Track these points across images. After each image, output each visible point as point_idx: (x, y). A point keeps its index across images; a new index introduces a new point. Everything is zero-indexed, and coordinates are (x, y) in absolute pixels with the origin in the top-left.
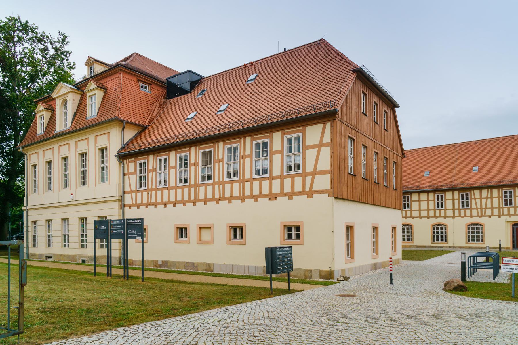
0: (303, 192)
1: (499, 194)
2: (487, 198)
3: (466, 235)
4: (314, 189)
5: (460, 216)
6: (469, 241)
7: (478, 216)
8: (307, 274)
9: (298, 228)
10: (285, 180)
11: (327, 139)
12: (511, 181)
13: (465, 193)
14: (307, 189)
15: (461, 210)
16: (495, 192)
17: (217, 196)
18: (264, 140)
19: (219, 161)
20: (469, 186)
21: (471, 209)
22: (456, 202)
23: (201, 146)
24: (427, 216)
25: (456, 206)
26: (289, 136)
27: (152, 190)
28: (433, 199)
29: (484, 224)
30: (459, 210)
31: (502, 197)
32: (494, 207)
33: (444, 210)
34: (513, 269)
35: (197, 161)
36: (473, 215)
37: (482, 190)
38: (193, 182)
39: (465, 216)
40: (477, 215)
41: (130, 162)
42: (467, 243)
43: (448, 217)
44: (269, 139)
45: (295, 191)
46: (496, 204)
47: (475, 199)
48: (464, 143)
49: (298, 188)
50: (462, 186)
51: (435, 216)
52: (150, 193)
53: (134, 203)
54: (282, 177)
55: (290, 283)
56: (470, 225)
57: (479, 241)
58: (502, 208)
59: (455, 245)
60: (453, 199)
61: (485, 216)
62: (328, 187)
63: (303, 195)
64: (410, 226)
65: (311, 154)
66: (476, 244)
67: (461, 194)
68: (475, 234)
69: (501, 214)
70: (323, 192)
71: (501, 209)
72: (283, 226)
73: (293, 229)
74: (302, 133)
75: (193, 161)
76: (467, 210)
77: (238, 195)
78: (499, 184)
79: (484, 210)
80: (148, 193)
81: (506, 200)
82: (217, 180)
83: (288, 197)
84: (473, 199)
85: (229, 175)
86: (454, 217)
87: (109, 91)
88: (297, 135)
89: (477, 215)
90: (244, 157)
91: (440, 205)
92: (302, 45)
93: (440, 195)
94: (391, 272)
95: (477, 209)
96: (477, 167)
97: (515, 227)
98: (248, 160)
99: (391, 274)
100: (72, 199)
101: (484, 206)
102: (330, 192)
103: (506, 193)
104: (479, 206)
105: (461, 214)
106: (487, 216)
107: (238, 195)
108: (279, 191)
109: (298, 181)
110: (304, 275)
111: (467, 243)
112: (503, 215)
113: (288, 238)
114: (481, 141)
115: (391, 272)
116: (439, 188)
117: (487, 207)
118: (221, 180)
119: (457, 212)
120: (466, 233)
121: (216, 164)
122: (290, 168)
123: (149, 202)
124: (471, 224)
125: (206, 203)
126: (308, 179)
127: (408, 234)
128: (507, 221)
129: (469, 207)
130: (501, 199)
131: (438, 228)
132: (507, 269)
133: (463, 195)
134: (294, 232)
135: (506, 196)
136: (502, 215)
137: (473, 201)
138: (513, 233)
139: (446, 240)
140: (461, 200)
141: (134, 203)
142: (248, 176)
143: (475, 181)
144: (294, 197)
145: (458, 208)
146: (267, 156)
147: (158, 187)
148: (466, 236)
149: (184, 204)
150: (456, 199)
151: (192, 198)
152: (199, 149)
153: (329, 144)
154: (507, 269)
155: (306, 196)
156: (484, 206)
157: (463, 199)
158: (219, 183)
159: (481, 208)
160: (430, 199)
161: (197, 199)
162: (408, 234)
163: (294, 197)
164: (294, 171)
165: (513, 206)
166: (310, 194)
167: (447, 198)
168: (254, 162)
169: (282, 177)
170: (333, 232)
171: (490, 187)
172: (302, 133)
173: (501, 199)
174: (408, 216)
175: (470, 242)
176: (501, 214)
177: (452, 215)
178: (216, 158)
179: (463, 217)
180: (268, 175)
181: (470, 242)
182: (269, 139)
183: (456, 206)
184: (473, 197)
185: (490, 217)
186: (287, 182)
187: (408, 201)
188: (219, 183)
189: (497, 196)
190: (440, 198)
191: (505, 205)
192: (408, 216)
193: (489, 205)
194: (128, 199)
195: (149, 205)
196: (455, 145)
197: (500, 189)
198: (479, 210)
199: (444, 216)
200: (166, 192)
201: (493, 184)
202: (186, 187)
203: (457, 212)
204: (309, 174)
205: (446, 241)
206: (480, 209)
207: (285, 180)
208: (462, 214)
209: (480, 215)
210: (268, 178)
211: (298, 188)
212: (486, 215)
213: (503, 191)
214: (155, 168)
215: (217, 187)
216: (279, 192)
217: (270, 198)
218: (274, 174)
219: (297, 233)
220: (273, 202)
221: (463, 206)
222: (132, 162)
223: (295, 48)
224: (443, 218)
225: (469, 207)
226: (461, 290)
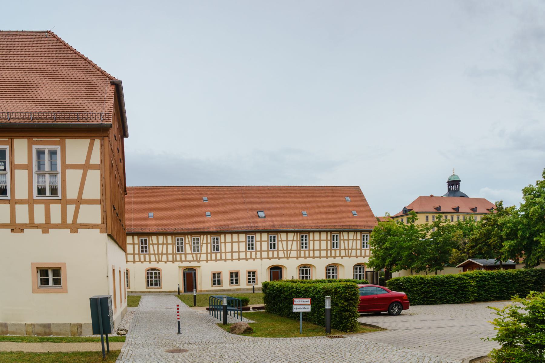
0: (63, 225)
1: (172, 241)
2: (163, 244)
3: (146, 280)
4: (79, 221)
5: (140, 261)
6: (148, 286)
7: (156, 261)
8: (75, 330)
9: (57, 272)
10: (35, 206)
11: (96, 159)
12: (182, 229)
13: (144, 238)
14: (70, 221)
15: (141, 255)
16: (169, 238)
18: (52, 147)
20: (148, 231)
21: (150, 254)
22: (136, 246)
24: (231, 258)
26: (41, 147)
28: (245, 241)
29: (161, 269)
30: (139, 254)
31: (175, 244)
32: (169, 253)
33: (219, 253)
34: (301, 308)
36: (152, 260)
37: (159, 236)
39: (145, 261)
40: (155, 260)
42: (147, 288)
44: (8, 146)
45: (51, 223)
46: (170, 251)
47: (344, 240)
48: (138, 188)
49: (56, 218)
50: (141, 231)
51: (268, 258)
54: (30, 202)
55: (109, 343)
56: (148, 270)
57: (153, 286)
58: (175, 254)
59: (136, 290)
61: (161, 261)
62: (98, 220)
63: (64, 228)
64: (158, 270)
66: (155, 288)
69: (175, 260)
70: (92, 226)
72: (36, 268)
73: (50, 273)
74: (60, 146)
76: (252, 252)
78: (173, 231)
79: (160, 256)
81: (178, 247)
83: (41, 230)
84: (280, 241)
86: (134, 262)
88: (52, 147)
89: (155, 260)
91: (335, 245)
92: (21, 30)
93: (273, 235)
94: (179, 320)
96: (152, 213)
97: (272, 271)
99: (179, 322)
101: (160, 252)
102: (101, 227)
103: (178, 240)
104: (156, 252)
105: (306, 255)
109: (55, 209)
110: (71, 332)
111: (147, 288)
112: (176, 261)
113: (54, 285)
114: (153, 188)
115: (179, 320)
116: (249, 230)
117: (163, 253)
119: (137, 257)
120: (146, 278)
122: (41, 191)
124: (150, 269)
127: (333, 275)
128: (180, 267)
129: (148, 253)
130: (299, 242)
131: (152, 272)
132: (297, 309)
133: (142, 240)
134: (51, 277)
135: (178, 244)
137: (342, 242)
138: (184, 277)
140: (270, 242)
143: (152, 226)
144: (50, 230)
145: (138, 253)
146: (5, 169)
148: (146, 281)
150: (136, 244)
153: (99, 167)
154: (297, 309)
155: (69, 230)
156: (160, 252)
159: (158, 254)
160: (240, 241)
162: (333, 275)
163: (50, 230)
164: (48, 195)
165: (184, 252)
166: (74, 228)
168: (35, 176)
170: (108, 276)
171: (165, 234)
172: (60, 146)
173: (299, 242)
175: (150, 287)
176: (175, 260)
177: (133, 260)
179: (142, 262)
182: (8, 146)
184: (151, 242)
185: (166, 262)
186: (39, 210)
187: (274, 241)
189: (171, 242)
190: (251, 239)
191: (142, 252)
193: (165, 252)
196: (129, 188)
197: (299, 233)
198: (157, 256)
199: (224, 259)
201: (167, 231)
204: (71, 202)
206: (157, 254)
207: (35, 206)
208: (142, 259)
209: (157, 260)
210: (8, 202)
211: (56, 218)
212: (163, 260)
213: (176, 238)
217: (12, 230)
218: (18, 197)
220: (17, 236)
221: (142, 251)
223: (10, 32)
224: (132, 263)
225: (184, 252)
226: (250, 333)
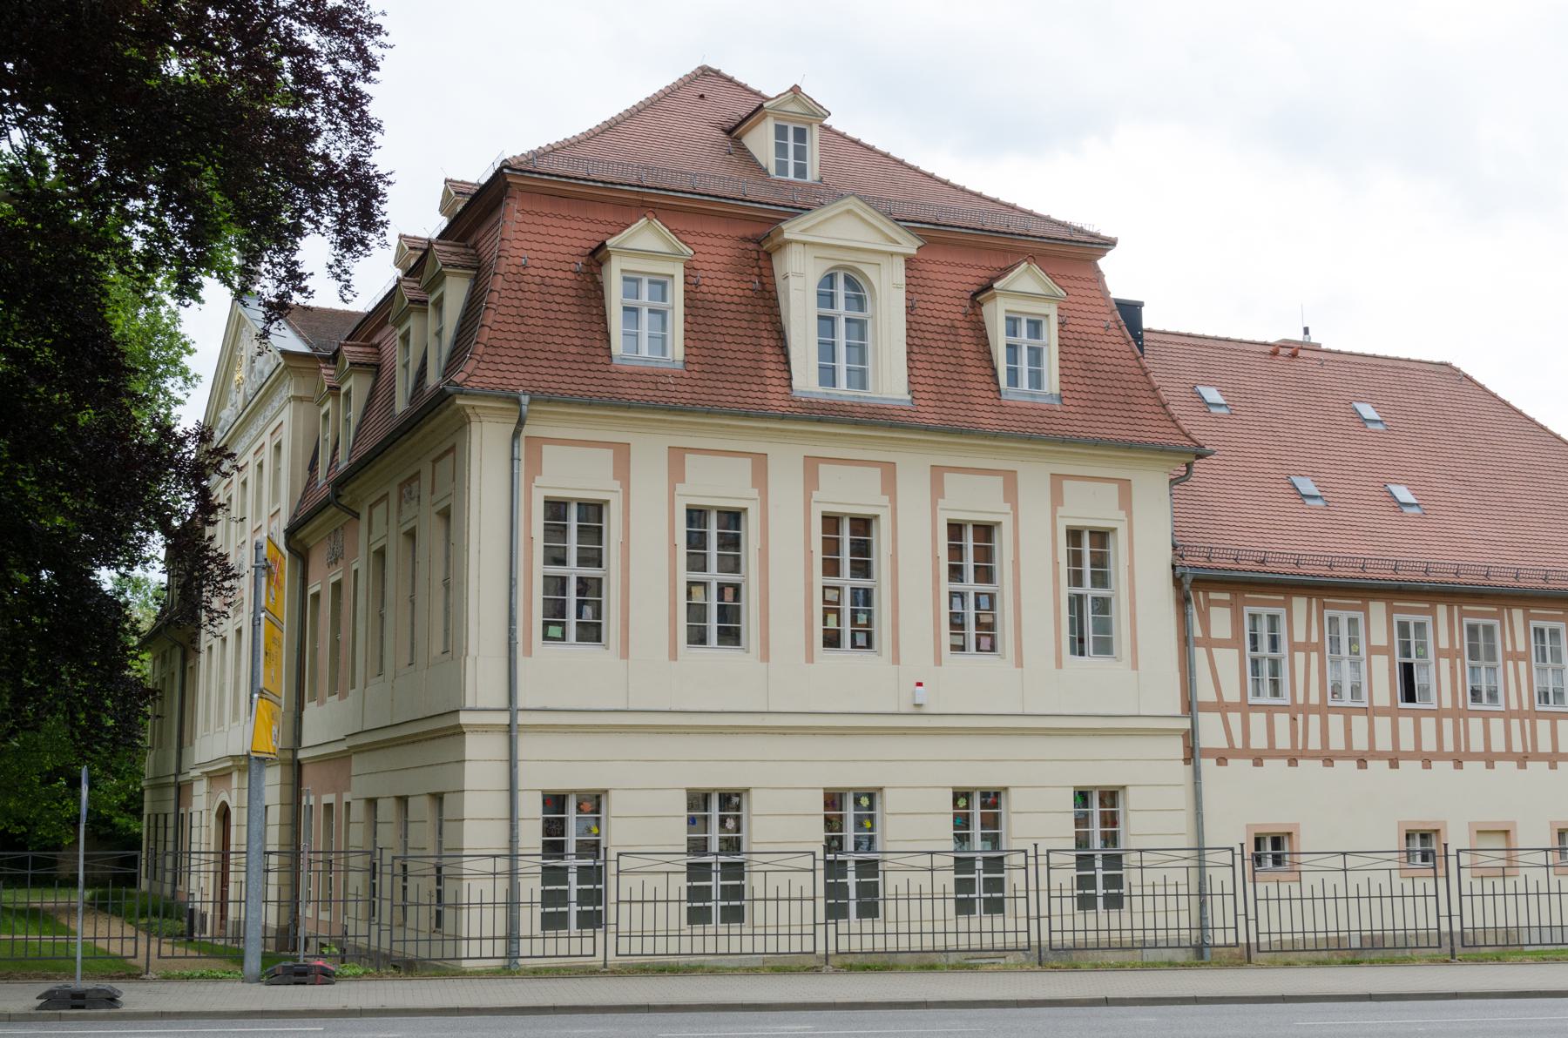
23: (1465, 608)
27: (1307, 709)
35: (1458, 647)
41: (1210, 603)
52: (1300, 717)
53: (1238, 744)
54: (1458, 714)
68: (851, 859)
82: (1514, 705)
87: (486, 252)
100: (919, 705)
118: (1300, 700)
123: (1300, 747)
125: (1394, 764)
147: (1251, 701)
149: (1427, 764)
151: (1449, 746)
152: (1462, 615)
155: (1484, 763)
158: (1520, 714)
161: (1463, 750)
169: (1458, 714)
178: (1509, 648)
188: (1520, 714)
195: (1302, 757)
200: (1360, 722)
215: (1515, 723)
222: (1219, 603)
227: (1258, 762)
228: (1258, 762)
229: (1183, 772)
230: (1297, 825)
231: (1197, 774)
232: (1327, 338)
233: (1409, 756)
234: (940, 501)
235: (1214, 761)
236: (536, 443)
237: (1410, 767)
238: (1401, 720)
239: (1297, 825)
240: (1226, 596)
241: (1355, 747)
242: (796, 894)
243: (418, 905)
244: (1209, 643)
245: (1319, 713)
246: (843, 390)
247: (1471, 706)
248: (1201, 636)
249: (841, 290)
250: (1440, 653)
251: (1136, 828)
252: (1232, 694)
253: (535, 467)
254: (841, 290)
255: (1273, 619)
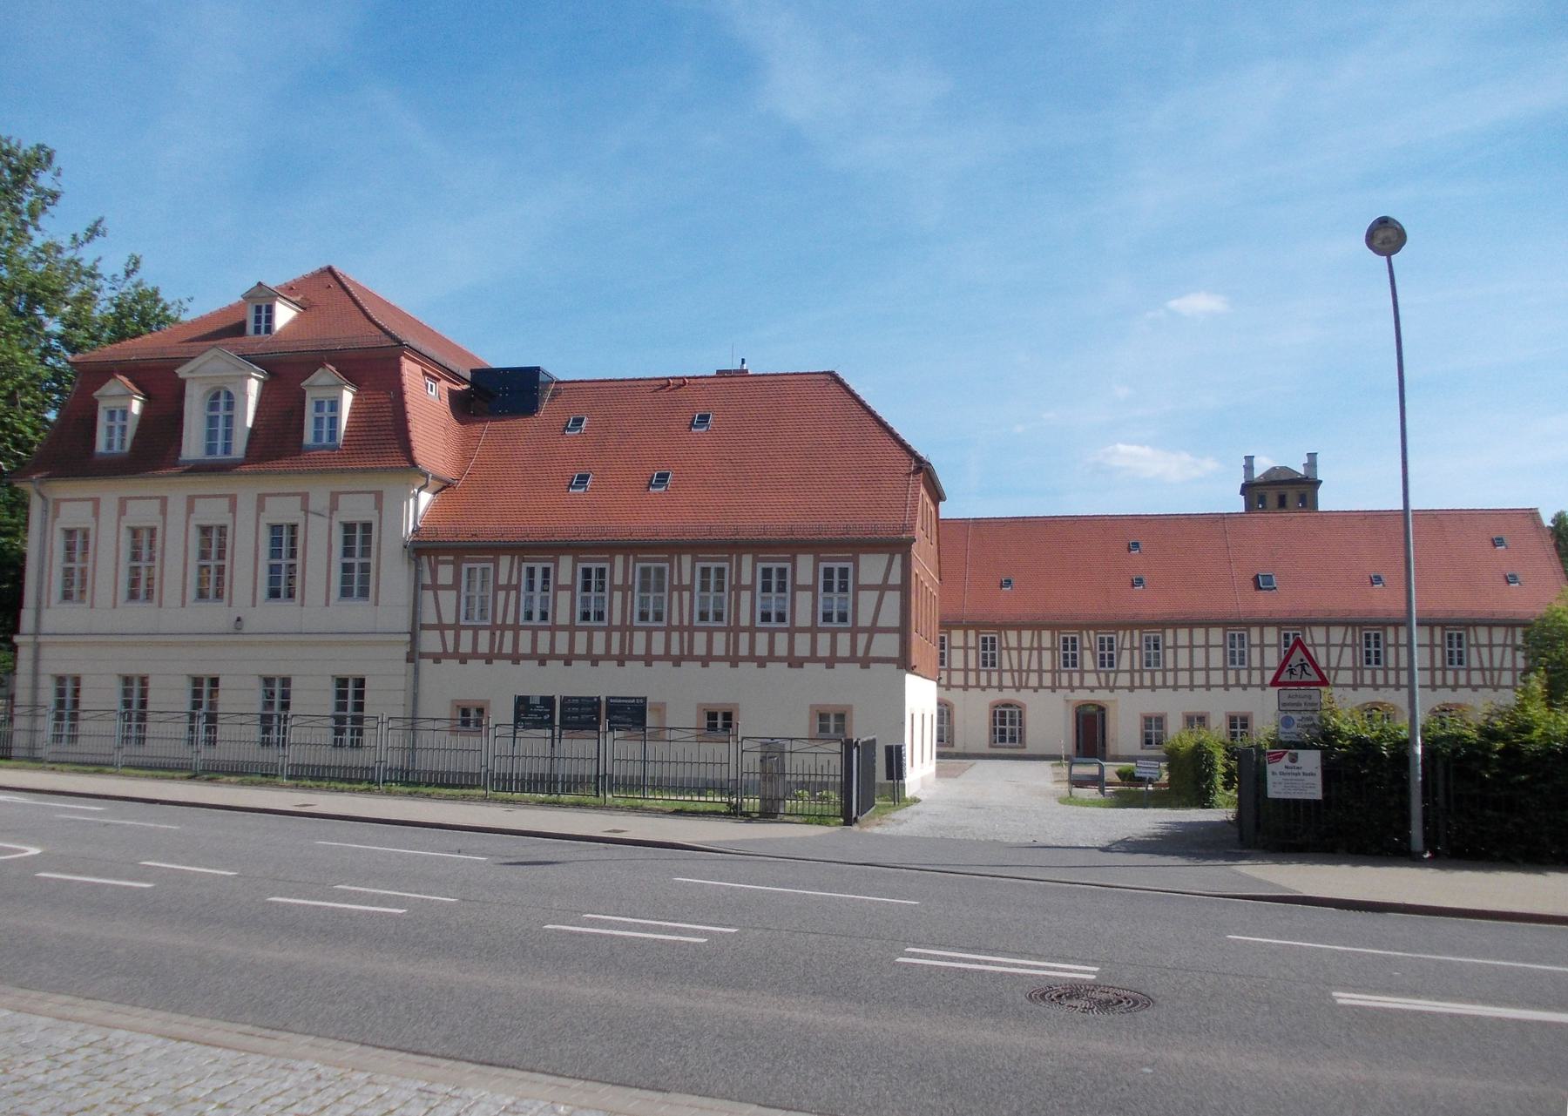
7: (1014, 687)
9: (728, 716)
14: (860, 653)
17: (675, 651)
19: (681, 588)
22: (972, 653)
25: (972, 665)
27: (504, 627)
30: (977, 671)
35: (630, 583)
38: (617, 621)
39: (989, 686)
41: (438, 562)
43: (953, 686)
46: (1047, 665)
52: (498, 633)
53: (450, 649)
60: (966, 648)
61: (1027, 687)
65: (867, 600)
67: (981, 636)
71: (1057, 675)
75: (618, 580)
77: (723, 653)
80: (494, 634)
81: (1066, 656)
82: (675, 622)
85: (704, 616)
86: (966, 687)
90: (738, 588)
95: (1012, 670)
98: (746, 596)
101: (1025, 667)
104: (1016, 667)
106: (1031, 688)
107: (723, 653)
108: (807, 653)
111: (991, 746)
119: (972, 676)
121: (675, 594)
126: (862, 639)
129: (997, 668)
130: (1056, 652)
136: (1057, 688)
139: (1020, 738)
140: (981, 652)
141: (450, 649)
142: (745, 621)
151: (615, 650)
152: (636, 560)
155: (859, 665)
157: (985, 648)
158: (681, 628)
159: (1020, 671)
166: (866, 662)
167: (953, 645)
173: (1056, 652)
174: (715, 653)
175: (998, 743)
179: (984, 689)
180: (786, 625)
181: (998, 743)
183: (972, 665)
185: (1036, 690)
188: (681, 628)
192: (715, 653)
193: (1034, 666)
194: (430, 642)
195: (497, 658)
198: (1016, 674)
202: (485, 628)
203: (972, 676)
204: (864, 630)
205: (1020, 741)
209: (1017, 684)
214: (514, 582)
216: (715, 633)
218: (798, 624)
219: (282, 702)
227: (542, 662)
228: (542, 662)
229: (402, 667)
230: (488, 702)
231: (416, 671)
232: (752, 368)
233: (580, 658)
234: (262, 514)
235: (431, 661)
236: (57, 502)
237: (555, 666)
238: (446, 632)
239: (488, 702)
240: (451, 558)
241: (539, 651)
242: (717, 760)
243: (754, 773)
244: (435, 587)
245: (513, 630)
246: (219, 455)
247: (637, 623)
248: (430, 583)
249: (222, 401)
250: (672, 588)
251: (374, 703)
252: (449, 618)
253: (56, 515)
254: (222, 401)
255: (782, 572)
